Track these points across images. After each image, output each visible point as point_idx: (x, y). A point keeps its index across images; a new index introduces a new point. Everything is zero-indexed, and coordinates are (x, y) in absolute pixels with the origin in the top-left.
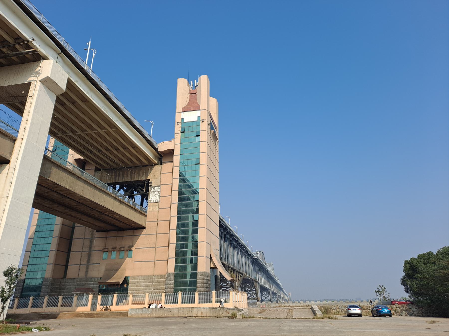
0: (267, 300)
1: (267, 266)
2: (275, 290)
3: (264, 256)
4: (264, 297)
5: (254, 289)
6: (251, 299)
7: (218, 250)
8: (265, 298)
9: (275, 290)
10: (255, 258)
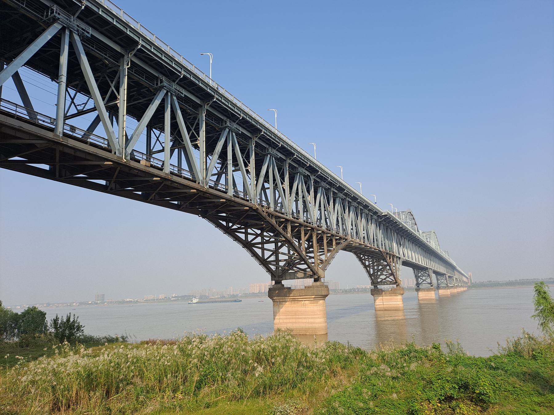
0: (425, 284)
1: (423, 238)
2: (442, 269)
3: (414, 219)
4: (422, 279)
5: (388, 267)
6: (385, 283)
7: (23, 107)
8: (422, 280)
9: (442, 269)
10: (383, 214)
